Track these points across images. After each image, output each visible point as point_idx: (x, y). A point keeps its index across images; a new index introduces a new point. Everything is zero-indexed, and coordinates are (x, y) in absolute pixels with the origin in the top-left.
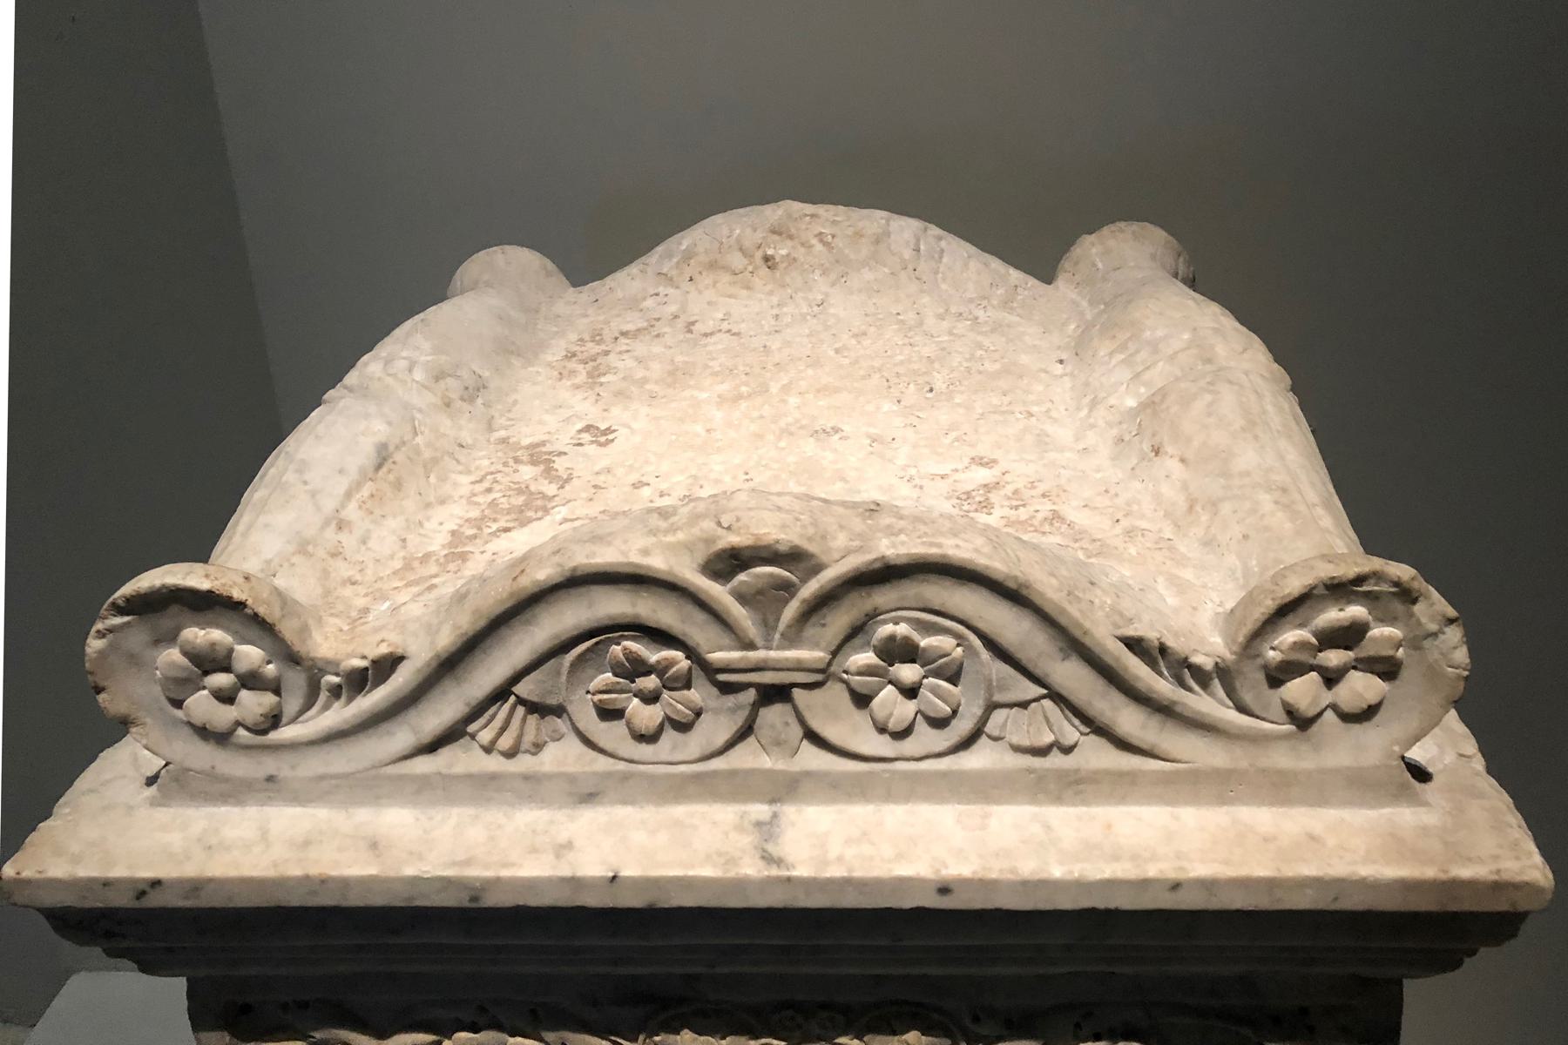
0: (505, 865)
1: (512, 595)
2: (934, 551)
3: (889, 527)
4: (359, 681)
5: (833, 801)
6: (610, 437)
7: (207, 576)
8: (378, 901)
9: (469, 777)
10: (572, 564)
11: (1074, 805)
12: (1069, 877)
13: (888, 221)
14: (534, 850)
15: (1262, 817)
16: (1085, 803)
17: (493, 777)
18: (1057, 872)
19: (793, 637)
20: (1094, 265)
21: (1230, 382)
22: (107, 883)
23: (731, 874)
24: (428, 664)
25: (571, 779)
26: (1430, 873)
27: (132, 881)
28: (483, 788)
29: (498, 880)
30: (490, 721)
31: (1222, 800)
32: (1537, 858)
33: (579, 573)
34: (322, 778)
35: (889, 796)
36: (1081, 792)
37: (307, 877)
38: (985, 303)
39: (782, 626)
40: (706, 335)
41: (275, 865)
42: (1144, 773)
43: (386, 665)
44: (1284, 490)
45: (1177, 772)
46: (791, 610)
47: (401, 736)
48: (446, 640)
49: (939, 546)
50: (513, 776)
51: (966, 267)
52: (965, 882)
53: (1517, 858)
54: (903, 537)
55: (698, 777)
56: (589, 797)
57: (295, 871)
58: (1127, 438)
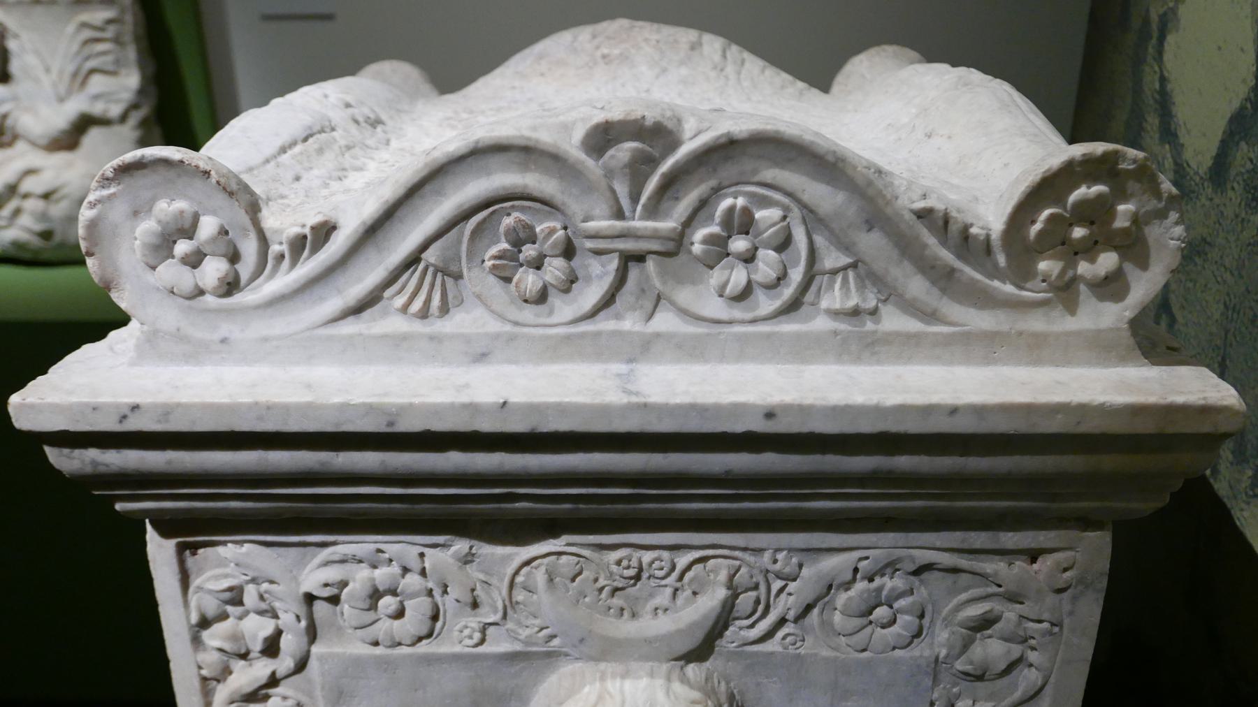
1: (426, 165)
8: (300, 473)
9: (384, 337)
10: (475, 138)
13: (700, 37)
16: (879, 362)
17: (405, 337)
19: (653, 211)
25: (467, 339)
27: (117, 406)
29: (411, 405)
31: (988, 361)
33: (480, 145)
34: (266, 339)
36: (875, 353)
37: (257, 403)
39: (643, 199)
42: (927, 334)
43: (325, 231)
45: (954, 334)
48: (370, 209)
52: (788, 408)
55: (568, 338)
56: (482, 357)
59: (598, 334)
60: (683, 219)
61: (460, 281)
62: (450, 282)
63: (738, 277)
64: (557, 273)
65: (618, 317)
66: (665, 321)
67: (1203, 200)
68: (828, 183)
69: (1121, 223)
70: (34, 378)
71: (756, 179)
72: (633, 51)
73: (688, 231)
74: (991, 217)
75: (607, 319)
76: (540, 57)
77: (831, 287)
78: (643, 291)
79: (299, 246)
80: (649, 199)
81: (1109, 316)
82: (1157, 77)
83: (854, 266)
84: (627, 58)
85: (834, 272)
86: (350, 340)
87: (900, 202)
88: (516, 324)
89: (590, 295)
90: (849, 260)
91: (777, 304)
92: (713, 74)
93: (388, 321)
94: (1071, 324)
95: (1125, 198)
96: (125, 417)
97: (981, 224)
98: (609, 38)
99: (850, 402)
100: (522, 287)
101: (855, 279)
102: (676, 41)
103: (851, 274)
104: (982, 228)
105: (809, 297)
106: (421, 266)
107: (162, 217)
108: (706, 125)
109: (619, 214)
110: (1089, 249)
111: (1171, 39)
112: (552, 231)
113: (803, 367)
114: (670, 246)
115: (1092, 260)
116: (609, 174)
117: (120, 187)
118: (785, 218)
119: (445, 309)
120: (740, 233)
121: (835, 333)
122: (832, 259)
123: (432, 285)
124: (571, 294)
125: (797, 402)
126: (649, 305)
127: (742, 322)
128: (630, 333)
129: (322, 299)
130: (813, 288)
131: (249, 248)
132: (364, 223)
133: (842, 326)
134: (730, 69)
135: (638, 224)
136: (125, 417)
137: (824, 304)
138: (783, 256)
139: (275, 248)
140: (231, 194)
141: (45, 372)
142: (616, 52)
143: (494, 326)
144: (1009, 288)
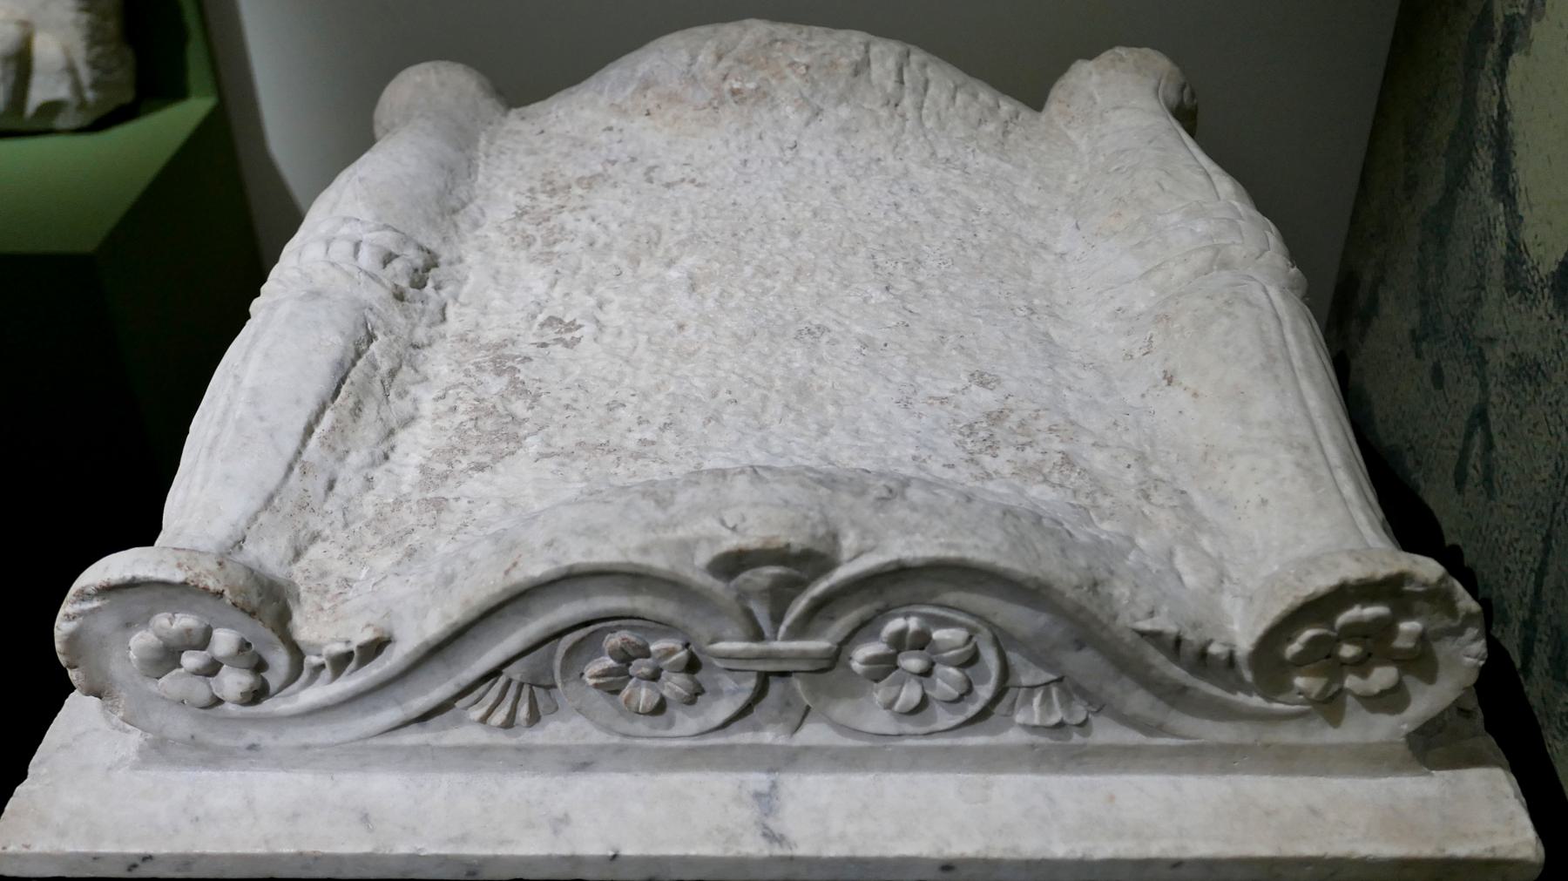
0: (502, 843)
1: (505, 590)
2: (953, 554)
3: (903, 522)
4: (341, 663)
5: (832, 770)
6: (577, 334)
7: (179, 566)
9: (457, 748)
11: (1077, 774)
12: (1071, 856)
14: (530, 825)
15: (1264, 788)
17: (484, 748)
18: (1059, 851)
19: (802, 628)
20: (1091, 97)
21: (1249, 303)
22: (96, 858)
23: (731, 854)
24: (416, 650)
25: (565, 750)
26: (1427, 851)
28: (474, 756)
30: (480, 698)
31: (1224, 769)
32: (1530, 833)
34: (306, 747)
35: (889, 767)
37: (301, 854)
38: (973, 145)
39: (788, 620)
40: (668, 185)
41: (267, 842)
43: (375, 648)
44: (1306, 449)
45: (1183, 747)
46: (800, 605)
47: (391, 714)
48: (434, 627)
49: (956, 547)
50: (505, 748)
51: (952, 101)
53: (1512, 834)
54: (918, 537)
55: (692, 751)
56: (584, 766)
57: (287, 849)
58: (1137, 355)
59: (732, 747)
60: (839, 639)
61: (553, 691)
62: (539, 693)
63: (910, 694)
64: (678, 689)
65: (757, 728)
66: (814, 734)
67: (1541, 312)
68: (1027, 605)
69: (1401, 643)
70: (10, 794)
71: (934, 601)
72: (774, 82)
73: (846, 647)
74: (1241, 630)
75: (743, 730)
76: (646, 85)
77: (1028, 701)
78: (788, 704)
79: (341, 663)
80: (796, 621)
81: (1387, 728)
82: (1496, 99)
83: (1060, 680)
84: (765, 94)
85: (1033, 687)
86: (415, 751)
87: (1120, 622)
88: (626, 735)
89: (723, 709)
90: (1052, 677)
91: (960, 719)
92: (884, 113)
93: (466, 731)
94: (1331, 736)
95: (1410, 615)
96: (135, 866)
97: (1224, 638)
98: (739, 61)
99: (1048, 856)
100: (633, 704)
101: (1059, 694)
102: (833, 64)
103: (1054, 691)
104: (1225, 644)
105: (1001, 708)
106: (502, 680)
107: (164, 633)
108: (870, 542)
109: (758, 636)
110: (1362, 665)
111: (1516, 60)
112: (671, 652)
113: (992, 777)
114: (824, 664)
115: (1364, 674)
116: (743, 596)
117: (106, 602)
118: (970, 638)
119: (534, 718)
120: (913, 648)
121: (1033, 746)
122: (1028, 675)
123: (518, 697)
124: (696, 707)
125: (981, 855)
126: (796, 718)
127: (915, 735)
128: (770, 746)
129: (377, 709)
130: (1006, 700)
131: (279, 660)
132: (426, 643)
133: (1042, 740)
134: (908, 102)
135: (779, 645)
136: (135, 866)
137: (1020, 718)
138: (968, 671)
139: (312, 660)
140: (252, 614)
141: (22, 776)
142: (751, 86)
143: (598, 737)
144: (1256, 701)
